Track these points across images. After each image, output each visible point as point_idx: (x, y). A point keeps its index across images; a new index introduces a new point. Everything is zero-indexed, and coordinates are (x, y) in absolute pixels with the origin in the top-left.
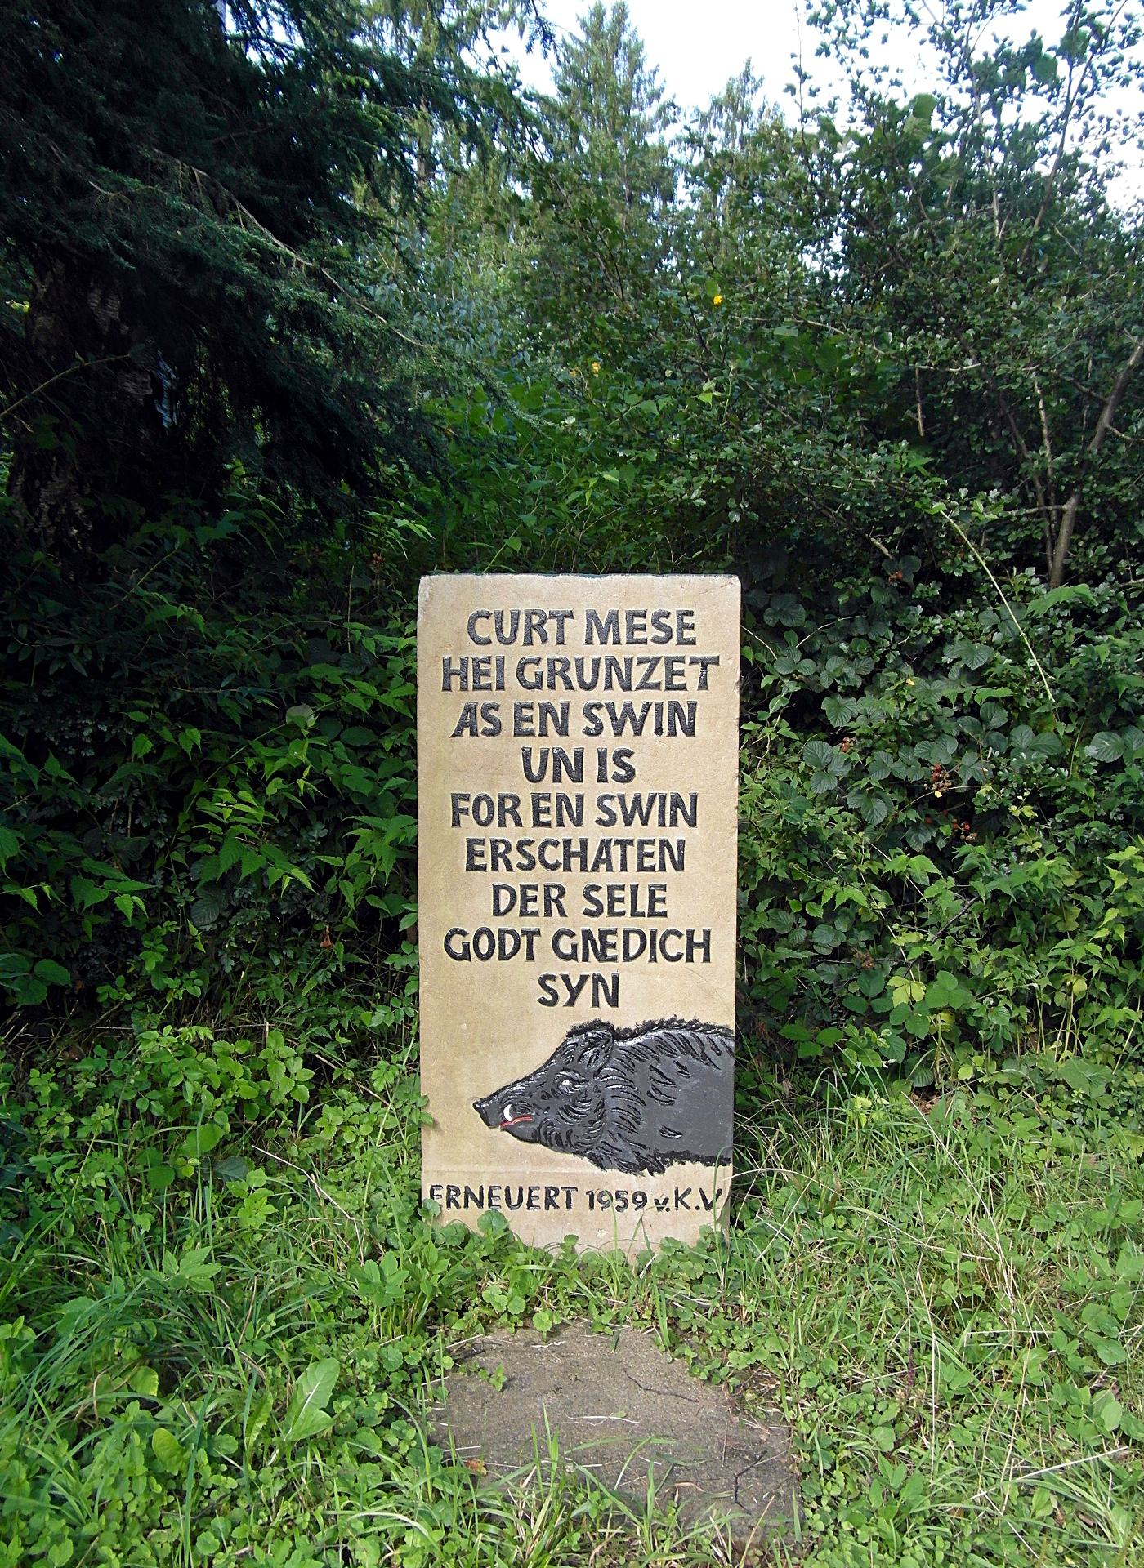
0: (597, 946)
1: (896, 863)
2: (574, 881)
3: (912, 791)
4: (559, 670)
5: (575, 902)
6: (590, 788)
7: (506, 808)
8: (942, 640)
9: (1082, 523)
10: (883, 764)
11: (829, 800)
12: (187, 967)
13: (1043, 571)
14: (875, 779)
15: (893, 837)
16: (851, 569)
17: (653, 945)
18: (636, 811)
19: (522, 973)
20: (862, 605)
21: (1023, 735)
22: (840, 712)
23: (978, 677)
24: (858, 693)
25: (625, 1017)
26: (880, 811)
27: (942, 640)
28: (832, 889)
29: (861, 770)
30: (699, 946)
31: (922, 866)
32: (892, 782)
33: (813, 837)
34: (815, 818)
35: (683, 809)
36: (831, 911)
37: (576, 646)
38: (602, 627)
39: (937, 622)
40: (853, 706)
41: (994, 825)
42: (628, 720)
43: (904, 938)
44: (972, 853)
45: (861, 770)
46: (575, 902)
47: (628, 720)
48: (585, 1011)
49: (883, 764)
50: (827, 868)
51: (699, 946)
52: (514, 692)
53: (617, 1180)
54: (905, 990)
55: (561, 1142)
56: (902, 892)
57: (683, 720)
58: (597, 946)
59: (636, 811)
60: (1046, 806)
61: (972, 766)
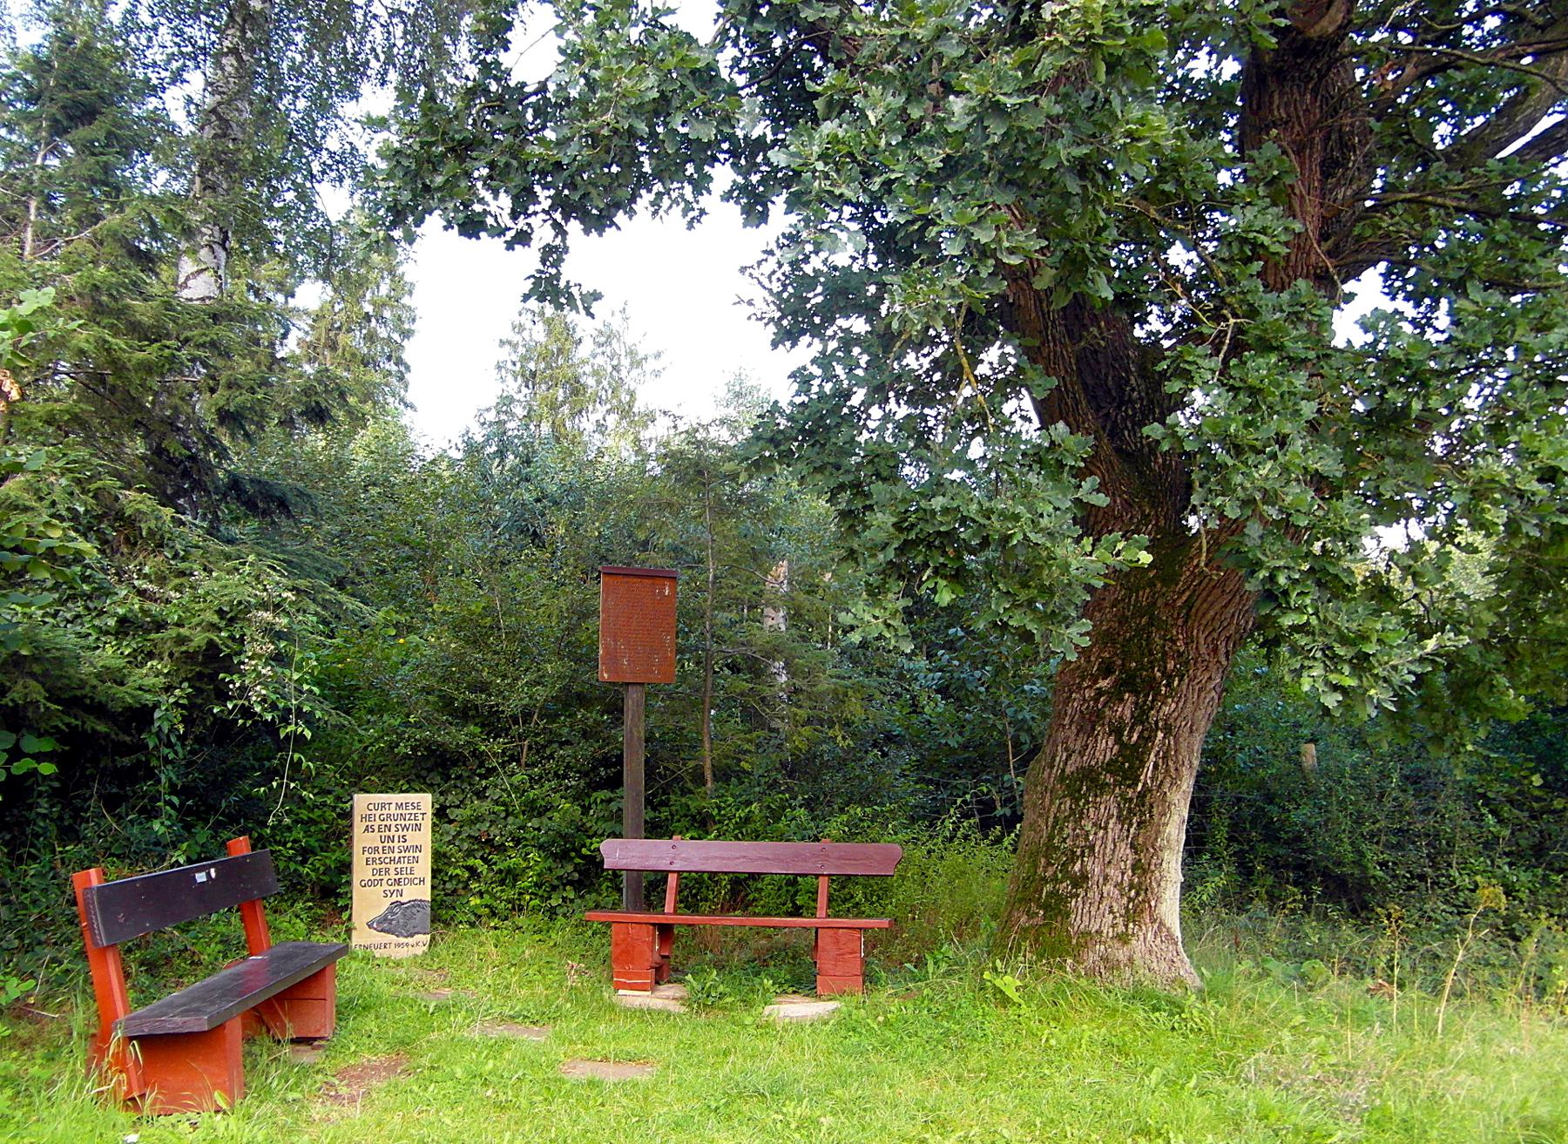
0: (398, 882)
1: (471, 862)
2: (392, 866)
3: (477, 839)
4: (389, 816)
5: (392, 872)
6: (396, 844)
7: (376, 850)
8: (486, 788)
9: (530, 748)
10: (467, 831)
11: (449, 843)
12: (1557, 612)
13: (519, 764)
14: (464, 836)
15: (470, 854)
16: (455, 764)
17: (411, 881)
18: (407, 849)
19: (379, 889)
20: (459, 777)
21: (511, 819)
22: (453, 813)
23: (496, 802)
24: (458, 807)
25: (403, 900)
26: (466, 846)
27: (486, 788)
28: (451, 871)
29: (459, 833)
30: (422, 881)
31: (479, 862)
32: (470, 836)
33: (445, 855)
34: (445, 849)
35: (418, 848)
36: (451, 877)
37: (393, 810)
38: (399, 806)
39: (484, 783)
40: (458, 811)
41: (501, 849)
42: (405, 828)
43: (474, 885)
44: (495, 858)
45: (459, 833)
46: (392, 872)
47: (405, 828)
48: (394, 899)
49: (467, 831)
50: (449, 864)
51: (422, 881)
52: (378, 822)
53: (402, 940)
54: (475, 901)
55: (388, 932)
56: (472, 870)
57: (418, 827)
58: (398, 882)
59: (407, 849)
60: (517, 841)
61: (494, 831)
